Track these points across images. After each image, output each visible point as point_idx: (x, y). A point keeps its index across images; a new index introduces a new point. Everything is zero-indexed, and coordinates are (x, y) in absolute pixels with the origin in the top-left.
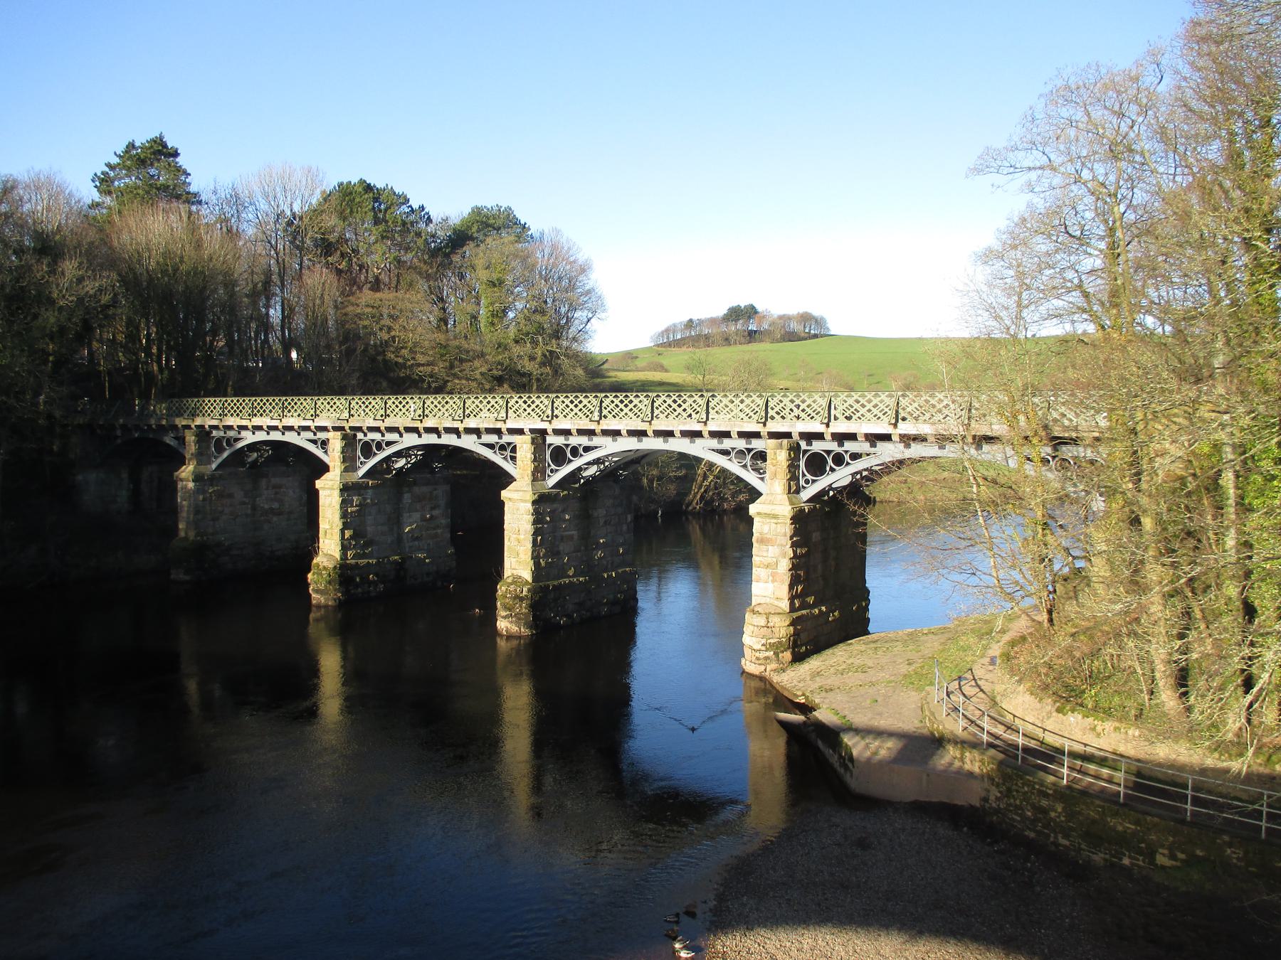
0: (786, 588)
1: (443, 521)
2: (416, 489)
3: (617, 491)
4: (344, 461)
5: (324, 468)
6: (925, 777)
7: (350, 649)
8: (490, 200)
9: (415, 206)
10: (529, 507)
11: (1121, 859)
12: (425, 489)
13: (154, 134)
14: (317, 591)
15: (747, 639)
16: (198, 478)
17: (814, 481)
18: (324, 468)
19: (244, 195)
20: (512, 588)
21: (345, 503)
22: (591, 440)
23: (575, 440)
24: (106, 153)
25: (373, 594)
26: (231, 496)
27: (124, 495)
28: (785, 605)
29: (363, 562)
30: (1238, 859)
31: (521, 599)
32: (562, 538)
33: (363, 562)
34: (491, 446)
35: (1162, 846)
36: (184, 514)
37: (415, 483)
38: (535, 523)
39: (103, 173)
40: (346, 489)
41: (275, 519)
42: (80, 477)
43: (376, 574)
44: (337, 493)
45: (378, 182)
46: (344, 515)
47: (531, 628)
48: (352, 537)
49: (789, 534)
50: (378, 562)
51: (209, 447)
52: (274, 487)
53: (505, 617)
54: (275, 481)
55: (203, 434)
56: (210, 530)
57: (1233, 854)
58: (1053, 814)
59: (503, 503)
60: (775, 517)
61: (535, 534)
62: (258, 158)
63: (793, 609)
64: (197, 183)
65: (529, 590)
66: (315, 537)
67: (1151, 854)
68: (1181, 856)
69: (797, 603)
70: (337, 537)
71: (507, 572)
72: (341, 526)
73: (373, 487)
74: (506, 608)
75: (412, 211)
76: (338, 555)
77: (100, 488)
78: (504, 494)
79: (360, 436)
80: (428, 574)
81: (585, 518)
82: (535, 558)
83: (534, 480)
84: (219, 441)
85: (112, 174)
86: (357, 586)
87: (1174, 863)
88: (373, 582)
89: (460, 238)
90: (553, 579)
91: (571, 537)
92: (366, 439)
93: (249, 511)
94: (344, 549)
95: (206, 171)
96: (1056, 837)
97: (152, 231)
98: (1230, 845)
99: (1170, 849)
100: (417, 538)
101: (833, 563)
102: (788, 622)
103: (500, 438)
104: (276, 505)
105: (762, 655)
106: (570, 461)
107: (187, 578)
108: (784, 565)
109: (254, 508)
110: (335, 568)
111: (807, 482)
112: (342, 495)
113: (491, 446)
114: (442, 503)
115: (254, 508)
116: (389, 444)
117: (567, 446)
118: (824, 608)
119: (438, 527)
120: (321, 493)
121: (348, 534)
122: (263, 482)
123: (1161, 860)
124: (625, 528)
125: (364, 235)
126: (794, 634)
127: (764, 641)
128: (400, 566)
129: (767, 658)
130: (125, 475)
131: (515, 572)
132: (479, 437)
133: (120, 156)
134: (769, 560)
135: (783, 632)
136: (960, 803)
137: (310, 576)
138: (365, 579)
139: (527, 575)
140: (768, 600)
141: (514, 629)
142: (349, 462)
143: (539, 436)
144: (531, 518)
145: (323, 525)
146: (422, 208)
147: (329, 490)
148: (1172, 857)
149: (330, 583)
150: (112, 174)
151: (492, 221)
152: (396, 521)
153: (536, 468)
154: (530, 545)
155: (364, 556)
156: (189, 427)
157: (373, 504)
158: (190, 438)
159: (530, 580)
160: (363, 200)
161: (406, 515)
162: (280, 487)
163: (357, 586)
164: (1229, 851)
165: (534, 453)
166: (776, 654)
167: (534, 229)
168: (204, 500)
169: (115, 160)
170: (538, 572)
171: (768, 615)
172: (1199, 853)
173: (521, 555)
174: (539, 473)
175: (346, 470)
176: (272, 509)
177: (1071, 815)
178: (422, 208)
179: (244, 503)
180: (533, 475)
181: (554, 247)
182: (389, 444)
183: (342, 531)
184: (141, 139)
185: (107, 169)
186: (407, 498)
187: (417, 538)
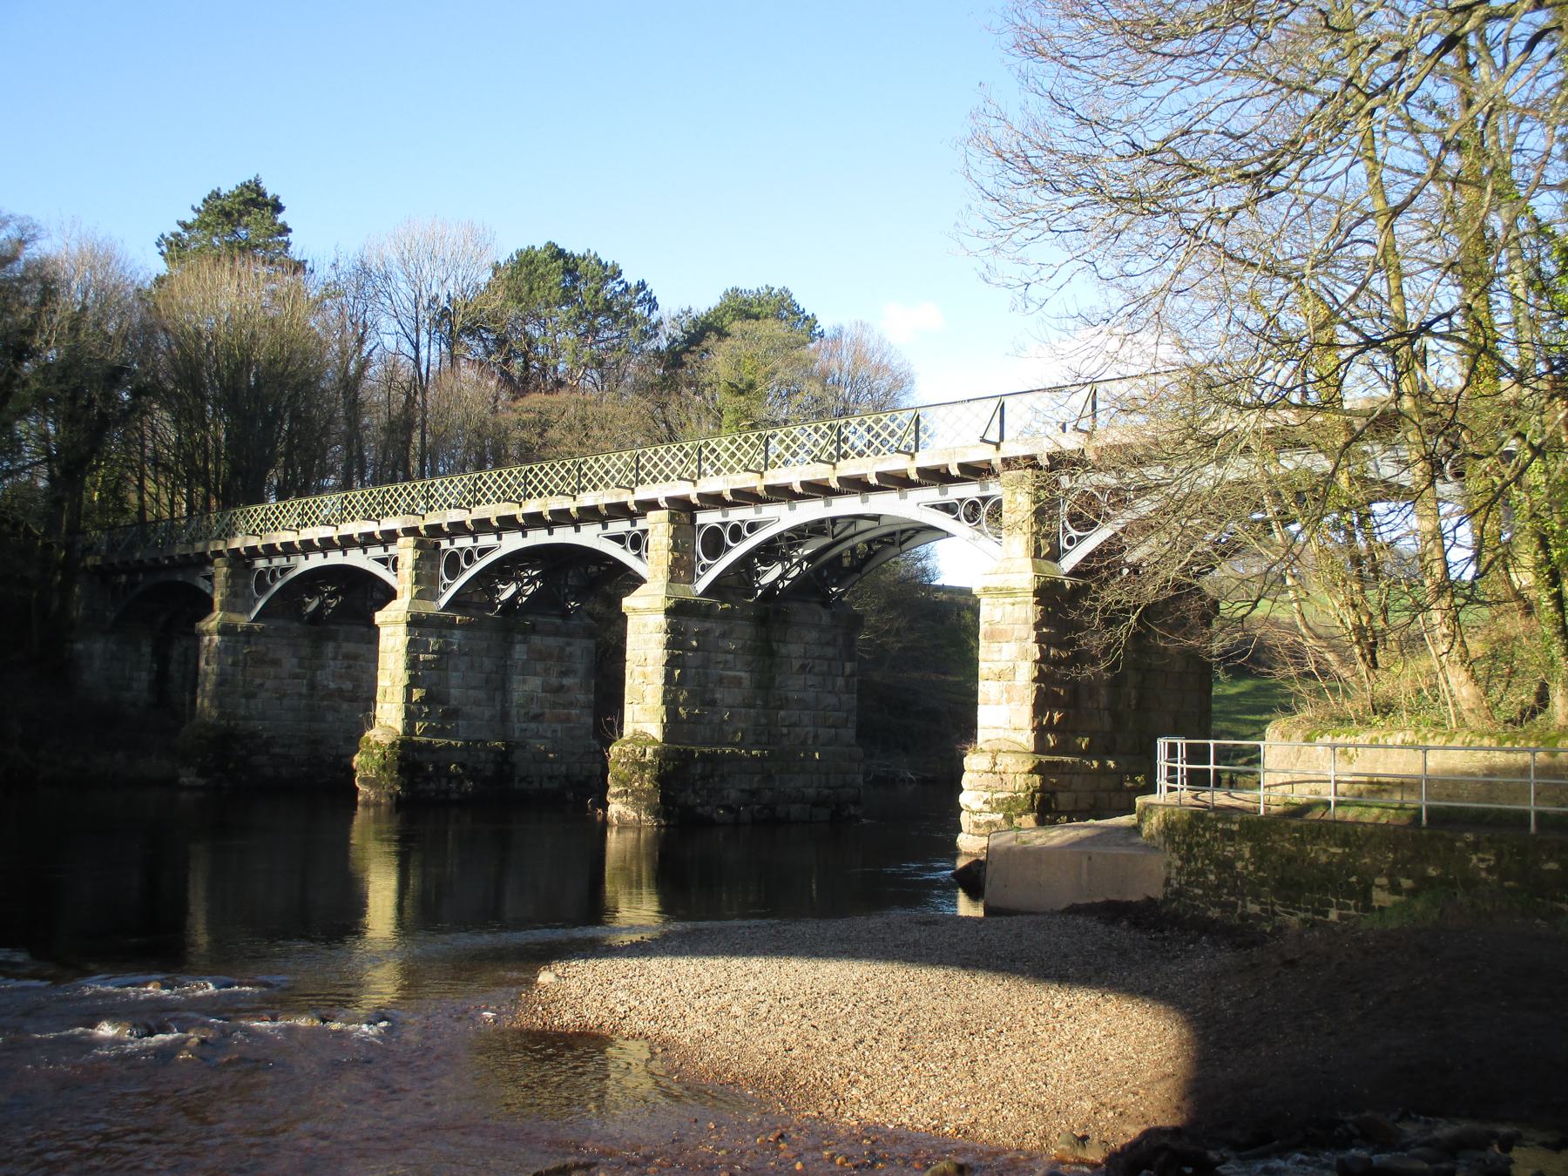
0: (1026, 711)
1: (581, 697)
2: (536, 640)
3: (826, 619)
4: (417, 582)
5: (390, 594)
6: (1085, 863)
7: (413, 882)
8: (752, 282)
9: (633, 283)
10: (661, 620)
11: (1326, 914)
12: (552, 642)
13: (247, 176)
14: (364, 781)
15: (964, 799)
16: (226, 630)
17: (1080, 539)
18: (390, 594)
19: (374, 263)
20: (628, 748)
21: (413, 647)
22: (758, 512)
23: (736, 515)
24: (179, 206)
25: (455, 796)
26: (276, 663)
27: (142, 680)
28: (1027, 739)
29: (440, 742)
30: (1489, 870)
31: (643, 767)
32: (721, 680)
33: (440, 742)
34: (619, 539)
35: (1380, 872)
36: (208, 687)
37: (533, 629)
38: (670, 645)
39: (173, 235)
40: (416, 623)
41: (345, 706)
42: (79, 646)
43: (463, 766)
44: (402, 628)
45: (574, 247)
46: (412, 664)
47: (656, 814)
48: (423, 701)
49: (1032, 620)
50: (466, 748)
51: (248, 585)
52: (347, 657)
53: (616, 795)
54: (348, 647)
55: (241, 562)
56: (242, 712)
57: (1481, 862)
58: (1239, 865)
59: (624, 618)
60: (1010, 592)
61: (670, 664)
62: (394, 219)
63: (1040, 747)
64: (301, 244)
65: (656, 753)
66: (369, 700)
67: (1363, 894)
68: (1406, 883)
69: (1051, 740)
70: (399, 697)
71: (628, 730)
72: (406, 681)
73: (462, 626)
74: (617, 780)
75: (627, 288)
76: (399, 727)
77: (105, 662)
78: (627, 603)
79: (445, 544)
80: (550, 778)
81: (764, 653)
82: (670, 702)
83: (673, 579)
84: (262, 574)
85: (186, 236)
86: (428, 779)
87: (1397, 898)
88: (456, 776)
89: (702, 332)
90: (704, 743)
91: (738, 682)
92: (453, 548)
93: (304, 690)
94: (410, 716)
95: (322, 235)
96: (1244, 906)
97: (226, 298)
98: (1476, 847)
99: (1390, 876)
100: (537, 718)
101: (1133, 693)
102: (1029, 766)
103: (633, 524)
104: (348, 685)
105: (983, 819)
106: (729, 548)
107: (201, 782)
108: (1026, 672)
109: (312, 686)
110: (393, 745)
111: (1070, 541)
112: (409, 633)
113: (619, 539)
114: (581, 666)
115: (312, 686)
116: (483, 552)
117: (724, 524)
118: (1111, 763)
119: (571, 704)
120: (383, 632)
121: (417, 694)
122: (330, 648)
123: (1380, 897)
124: (840, 681)
125: (557, 338)
126: (1042, 789)
127: (987, 796)
128: (504, 760)
129: (990, 824)
130: (146, 649)
131: (639, 727)
132: (605, 527)
133: (198, 211)
134: (1002, 666)
135: (1021, 781)
136: (1134, 899)
137: (357, 758)
138: (441, 769)
139: (655, 731)
140: (1001, 734)
141: (631, 814)
142: (426, 584)
143: (682, 509)
144: (662, 638)
145: (383, 681)
146: (642, 286)
147: (392, 624)
148: (1395, 888)
149: (384, 768)
150: (186, 236)
151: (756, 310)
152: (498, 684)
153: (675, 560)
154: (660, 681)
155: (441, 733)
156: (219, 554)
157: (462, 653)
158: (221, 570)
159: (659, 737)
160: (561, 280)
161: (516, 678)
162: (356, 657)
163: (428, 779)
164: (1474, 858)
165: (674, 537)
166: (1009, 819)
167: (825, 323)
168: (234, 664)
169: (190, 217)
170: (673, 724)
171: (995, 754)
172: (1432, 872)
173: (649, 699)
174: (681, 568)
175: (419, 596)
176: (340, 690)
177: (1260, 857)
178: (642, 286)
179: (297, 676)
180: (671, 572)
181: (857, 343)
182: (483, 552)
183: (409, 689)
184: (228, 186)
185: (180, 230)
186: (520, 652)
187: (537, 718)
